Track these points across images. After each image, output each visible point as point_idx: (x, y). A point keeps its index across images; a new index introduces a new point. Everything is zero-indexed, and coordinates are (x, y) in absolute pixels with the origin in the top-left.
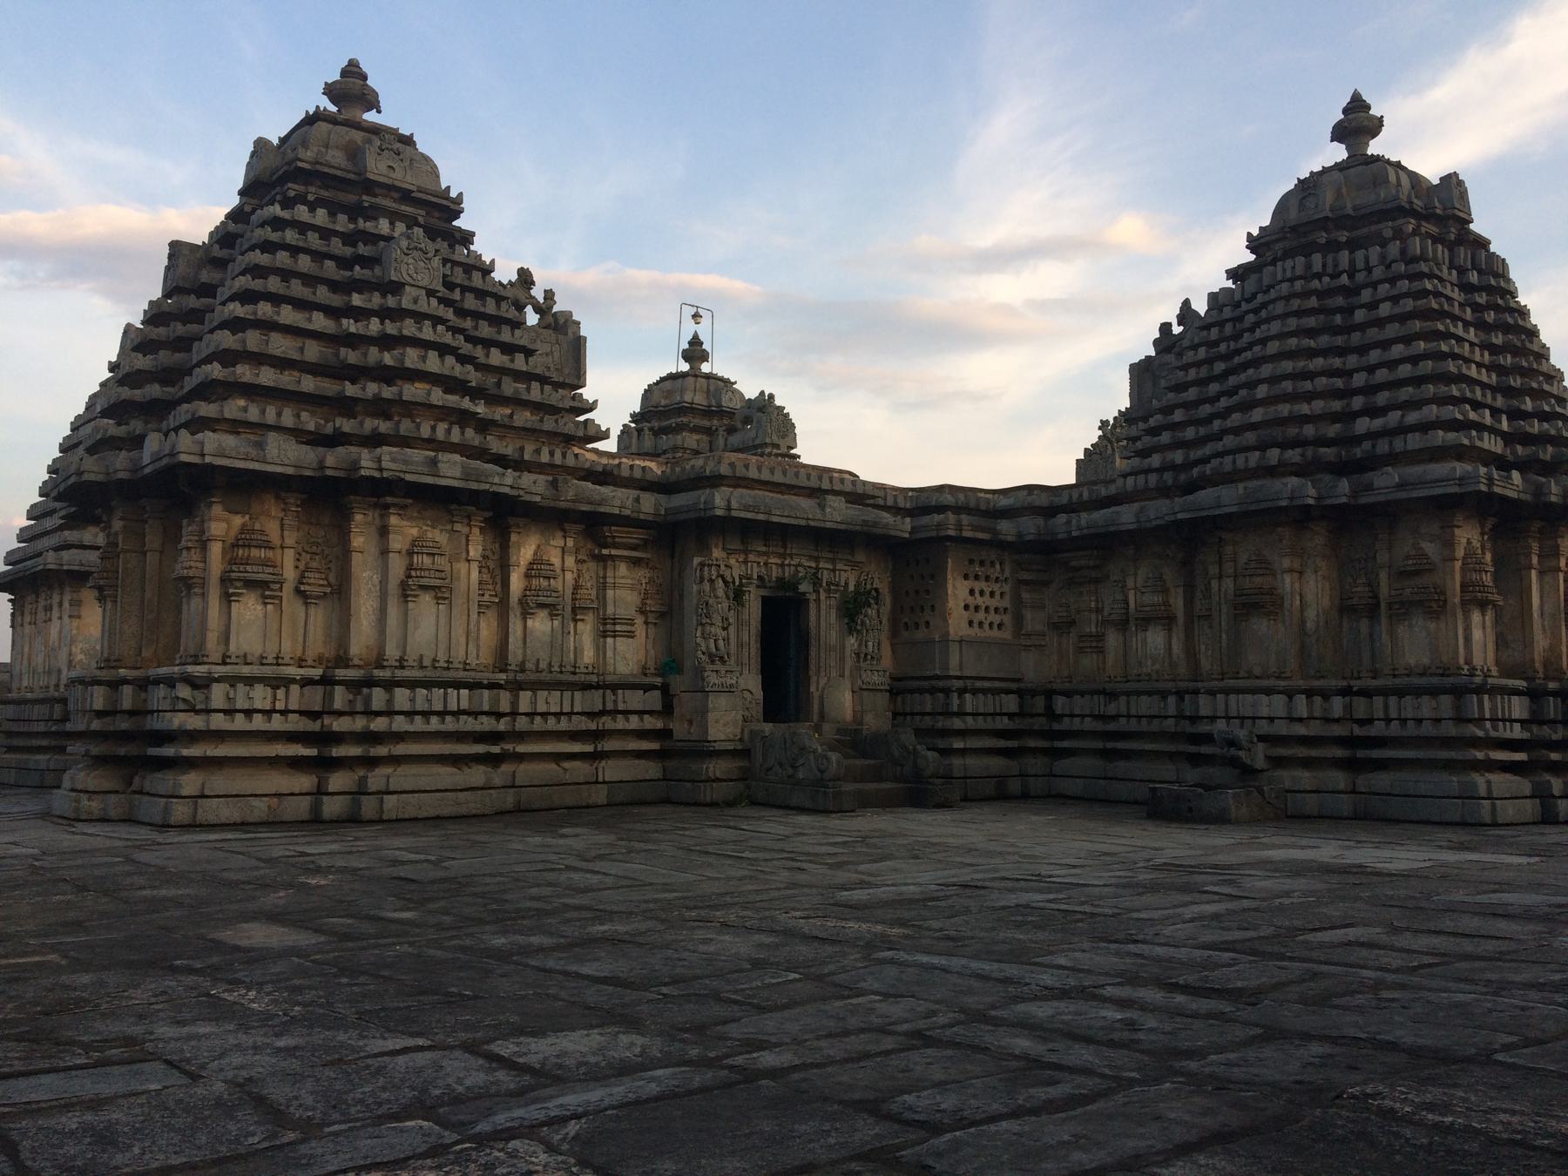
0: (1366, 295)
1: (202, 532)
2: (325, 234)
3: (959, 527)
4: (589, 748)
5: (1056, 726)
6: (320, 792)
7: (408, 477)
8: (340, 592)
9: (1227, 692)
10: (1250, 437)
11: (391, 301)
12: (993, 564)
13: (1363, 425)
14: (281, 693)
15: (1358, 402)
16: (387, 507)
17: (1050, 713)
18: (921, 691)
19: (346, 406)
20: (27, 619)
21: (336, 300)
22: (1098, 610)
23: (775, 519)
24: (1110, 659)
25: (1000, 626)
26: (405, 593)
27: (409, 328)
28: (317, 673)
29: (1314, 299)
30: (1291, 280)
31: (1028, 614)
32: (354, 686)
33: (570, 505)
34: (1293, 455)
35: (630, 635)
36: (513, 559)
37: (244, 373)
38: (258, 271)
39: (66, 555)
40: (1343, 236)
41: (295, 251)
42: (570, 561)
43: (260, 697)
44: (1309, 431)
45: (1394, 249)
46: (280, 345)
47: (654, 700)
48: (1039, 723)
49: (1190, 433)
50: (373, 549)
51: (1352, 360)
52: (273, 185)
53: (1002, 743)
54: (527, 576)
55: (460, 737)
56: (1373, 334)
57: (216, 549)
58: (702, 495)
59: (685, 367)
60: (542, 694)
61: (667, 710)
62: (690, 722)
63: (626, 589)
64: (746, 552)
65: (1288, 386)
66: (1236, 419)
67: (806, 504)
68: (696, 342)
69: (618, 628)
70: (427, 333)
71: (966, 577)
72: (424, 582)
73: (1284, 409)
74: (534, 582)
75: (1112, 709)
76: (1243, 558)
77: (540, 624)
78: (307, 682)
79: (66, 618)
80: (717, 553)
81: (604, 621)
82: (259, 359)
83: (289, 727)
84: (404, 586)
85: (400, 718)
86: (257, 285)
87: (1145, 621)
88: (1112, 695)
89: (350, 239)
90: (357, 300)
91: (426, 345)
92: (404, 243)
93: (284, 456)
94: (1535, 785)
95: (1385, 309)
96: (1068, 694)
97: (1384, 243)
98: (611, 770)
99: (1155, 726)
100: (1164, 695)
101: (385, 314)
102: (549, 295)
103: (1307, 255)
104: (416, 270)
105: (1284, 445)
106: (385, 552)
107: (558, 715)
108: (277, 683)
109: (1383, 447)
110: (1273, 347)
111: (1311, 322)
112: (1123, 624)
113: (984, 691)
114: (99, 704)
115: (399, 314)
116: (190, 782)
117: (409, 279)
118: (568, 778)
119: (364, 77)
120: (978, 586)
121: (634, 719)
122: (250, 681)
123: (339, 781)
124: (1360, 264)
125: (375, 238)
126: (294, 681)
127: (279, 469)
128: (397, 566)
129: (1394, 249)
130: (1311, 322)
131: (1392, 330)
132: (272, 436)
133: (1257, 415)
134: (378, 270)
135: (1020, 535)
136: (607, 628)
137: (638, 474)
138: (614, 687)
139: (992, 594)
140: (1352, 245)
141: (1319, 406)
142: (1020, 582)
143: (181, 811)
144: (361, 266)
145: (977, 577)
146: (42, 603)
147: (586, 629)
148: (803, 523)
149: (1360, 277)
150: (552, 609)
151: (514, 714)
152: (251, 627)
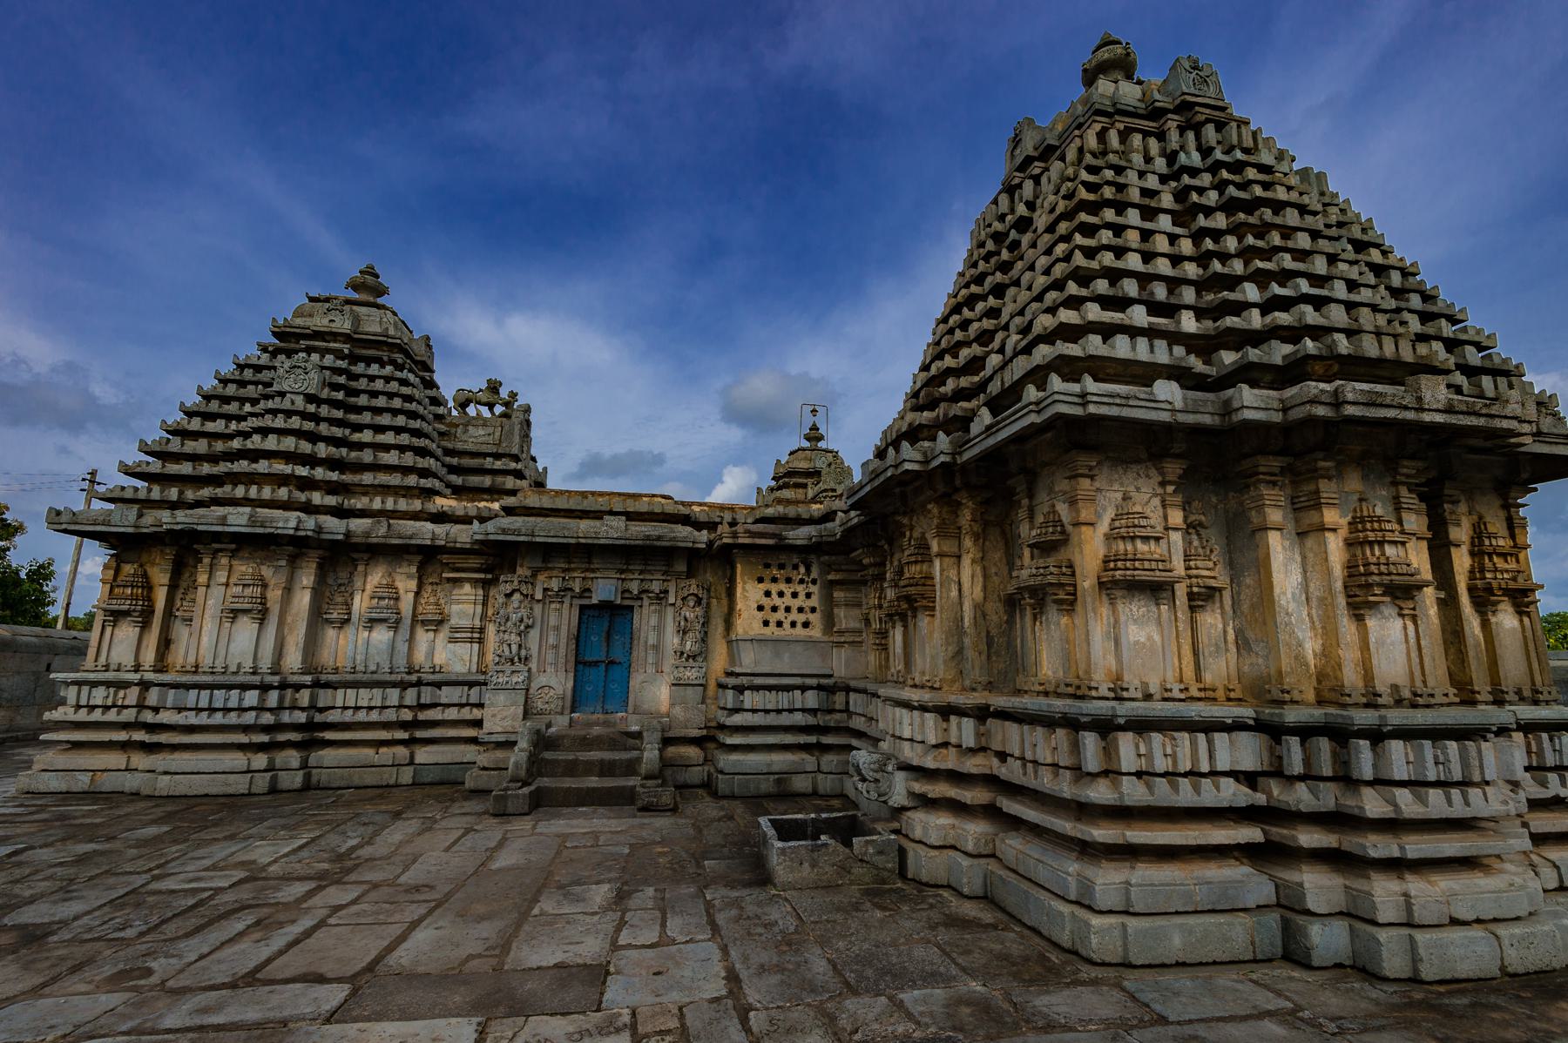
7: (200, 528)
12: (796, 567)
14: (121, 693)
23: (538, 539)
25: (806, 625)
31: (840, 612)
33: (382, 540)
53: (803, 739)
55: (246, 729)
59: (806, 444)
68: (814, 428)
78: (1237, 726)
102: (513, 395)
120: (774, 589)
122: (94, 684)
139: (795, 595)
142: (832, 582)
145: (774, 580)
148: (573, 541)
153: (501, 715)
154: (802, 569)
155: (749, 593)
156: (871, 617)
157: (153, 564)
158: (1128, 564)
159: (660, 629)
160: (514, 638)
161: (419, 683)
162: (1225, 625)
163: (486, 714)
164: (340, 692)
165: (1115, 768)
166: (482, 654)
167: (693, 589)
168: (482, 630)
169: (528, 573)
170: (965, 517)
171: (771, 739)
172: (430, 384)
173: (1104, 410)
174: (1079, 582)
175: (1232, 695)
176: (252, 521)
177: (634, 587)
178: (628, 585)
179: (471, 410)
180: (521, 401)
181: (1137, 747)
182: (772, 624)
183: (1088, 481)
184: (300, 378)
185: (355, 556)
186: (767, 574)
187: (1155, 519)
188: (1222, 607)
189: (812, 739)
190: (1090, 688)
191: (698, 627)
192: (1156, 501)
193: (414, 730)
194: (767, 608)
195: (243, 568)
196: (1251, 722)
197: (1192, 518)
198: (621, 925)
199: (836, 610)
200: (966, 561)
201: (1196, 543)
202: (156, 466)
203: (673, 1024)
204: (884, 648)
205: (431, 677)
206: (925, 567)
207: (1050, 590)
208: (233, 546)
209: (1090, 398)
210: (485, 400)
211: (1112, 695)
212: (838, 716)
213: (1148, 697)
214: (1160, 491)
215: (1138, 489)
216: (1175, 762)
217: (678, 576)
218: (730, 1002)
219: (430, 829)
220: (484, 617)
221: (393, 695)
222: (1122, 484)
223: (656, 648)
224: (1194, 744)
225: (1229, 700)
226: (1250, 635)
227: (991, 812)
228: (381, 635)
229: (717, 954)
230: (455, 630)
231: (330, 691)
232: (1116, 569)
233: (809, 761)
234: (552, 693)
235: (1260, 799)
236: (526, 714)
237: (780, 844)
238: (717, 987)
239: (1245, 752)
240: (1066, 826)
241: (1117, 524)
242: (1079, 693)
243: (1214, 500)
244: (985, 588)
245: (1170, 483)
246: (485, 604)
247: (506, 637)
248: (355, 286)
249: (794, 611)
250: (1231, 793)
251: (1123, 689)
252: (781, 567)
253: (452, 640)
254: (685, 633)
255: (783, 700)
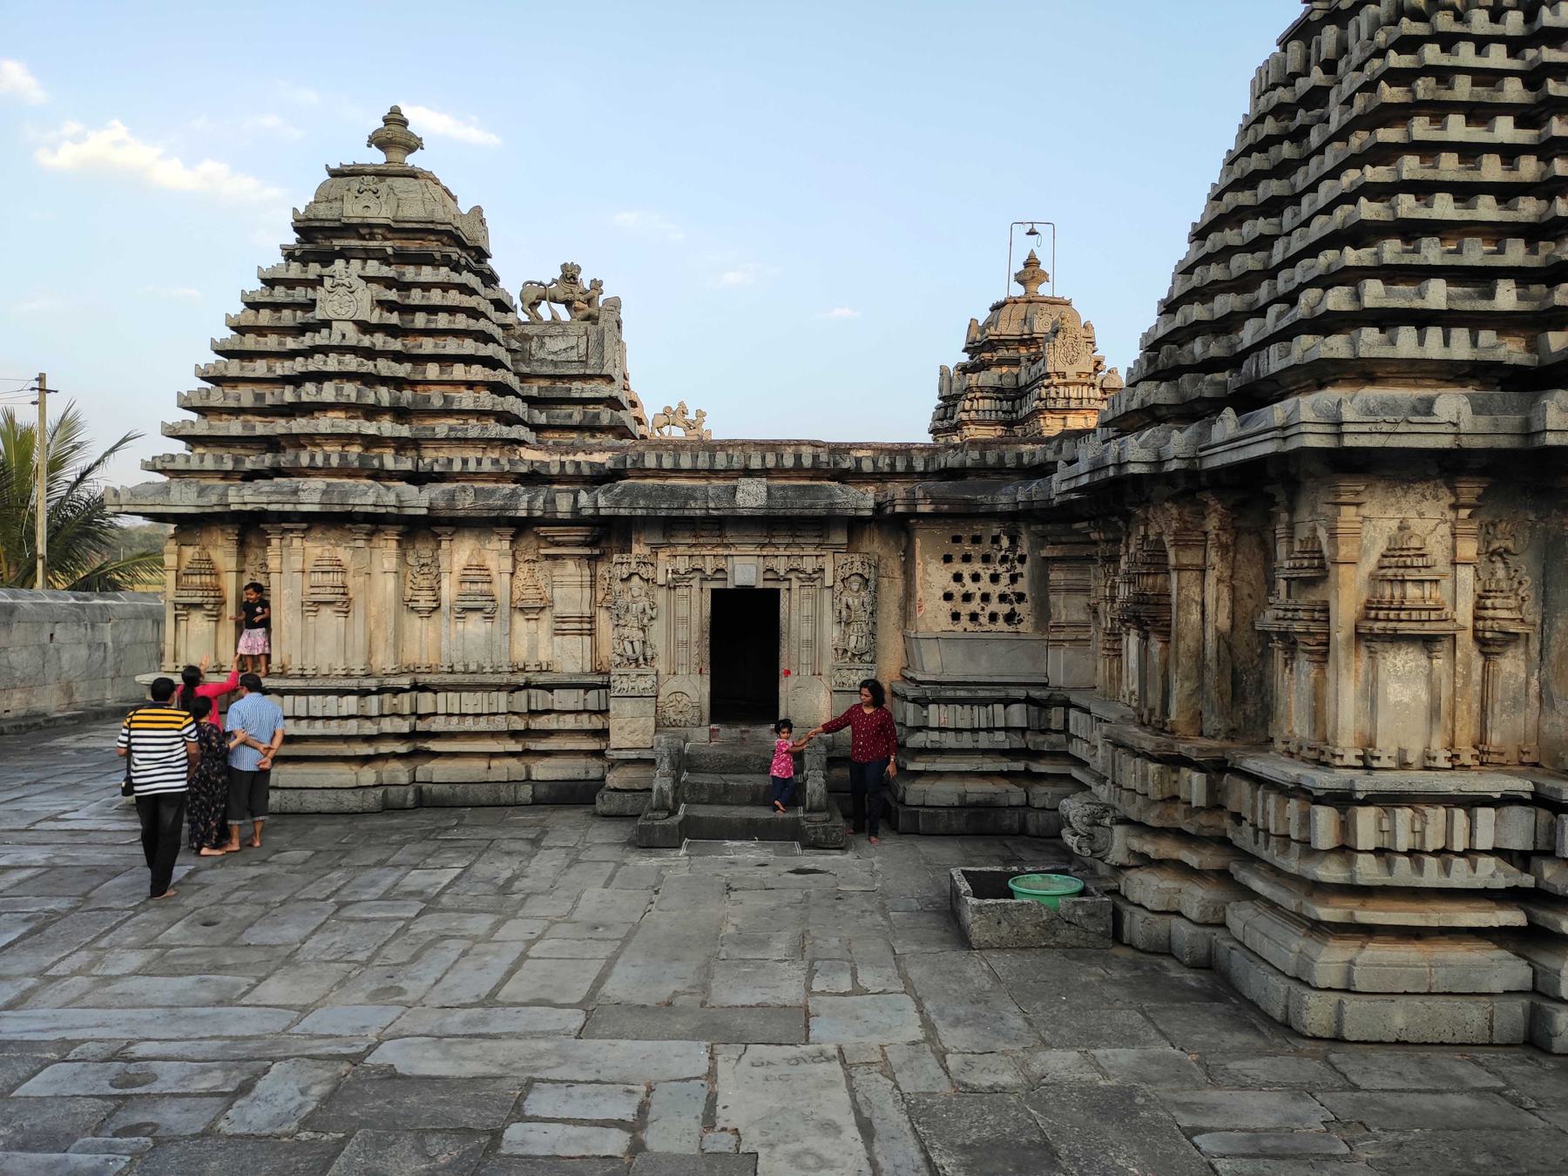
12: (996, 540)
25: (1010, 618)
29: (1270, 121)
36: (444, 565)
68: (1031, 262)
69: (578, 626)
71: (947, 559)
78: (1509, 800)
98: (543, 770)
117: (334, 316)
119: (405, 123)
120: (966, 570)
139: (995, 578)
142: (1046, 559)
145: (967, 559)
153: (630, 729)
154: (1005, 543)
155: (933, 576)
156: (1101, 609)
157: (216, 546)
158: (1392, 615)
159: (816, 619)
160: (637, 635)
161: (528, 685)
162: (1529, 674)
163: (613, 725)
164: (441, 696)
165: (1351, 844)
166: (595, 649)
167: (857, 568)
168: (592, 619)
169: (647, 551)
170: (1212, 524)
171: (964, 765)
172: (490, 279)
173: (1363, 442)
174: (1332, 632)
175: (1526, 759)
177: (781, 565)
178: (773, 563)
179: (544, 310)
180: (608, 292)
181: (1380, 823)
182: (965, 619)
183: (1353, 509)
184: (348, 297)
185: (438, 530)
186: (957, 551)
187: (1437, 549)
188: (1527, 653)
189: (1019, 766)
190: (1334, 756)
191: (865, 617)
192: (1445, 529)
193: (527, 739)
194: (958, 597)
195: (318, 551)
196: (1528, 796)
197: (1495, 545)
198: (811, 973)
199: (1052, 598)
200: (1211, 577)
201: (1501, 573)
202: (202, 427)
203: (877, 1058)
204: (1118, 654)
205: (542, 679)
206: (1160, 579)
207: (1299, 639)
208: (304, 525)
209: (1345, 428)
210: (561, 296)
211: (1360, 763)
212: (1054, 738)
213: (1404, 765)
214: (1450, 515)
215: (1421, 515)
216: (1423, 841)
217: (836, 549)
218: (927, 1047)
219: (577, 861)
220: (593, 602)
221: (501, 701)
222: (1400, 510)
223: (811, 644)
224: (1450, 820)
225: (1522, 764)
226: (1554, 689)
227: (1223, 876)
228: (475, 626)
229: (911, 1006)
230: (562, 619)
231: (429, 695)
232: (1377, 619)
233: (1015, 794)
234: (685, 700)
235: (1528, 881)
236: (659, 727)
237: (976, 901)
238: (916, 1033)
239: (1518, 830)
240: (1290, 901)
241: (1386, 562)
242: (1323, 759)
243: (1532, 517)
244: (1233, 615)
245: (1464, 506)
246: (593, 586)
247: (626, 631)
248: (378, 141)
249: (995, 599)
250: (1490, 873)
251: (1373, 758)
252: (976, 540)
253: (560, 632)
254: (848, 624)
255: (980, 716)
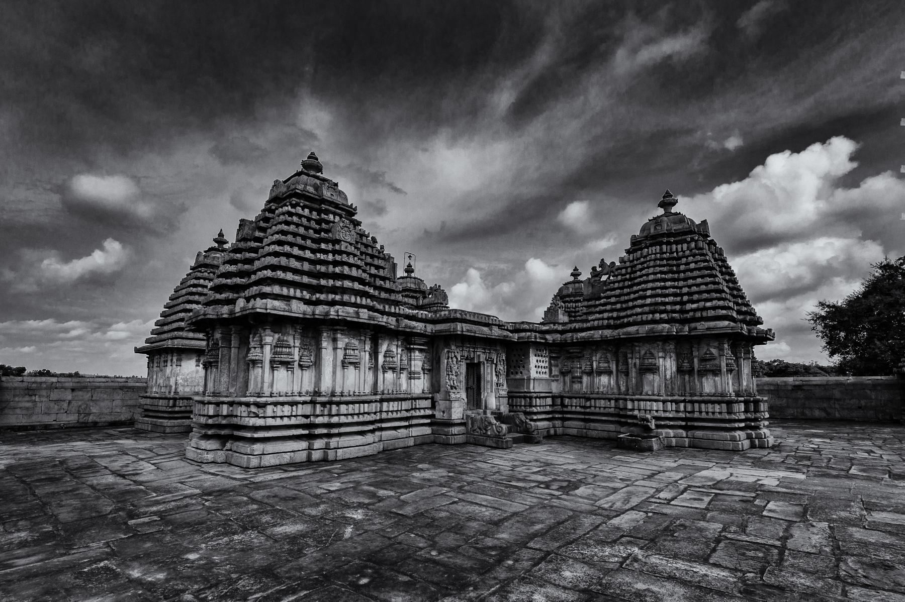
0: (684, 260)
1: (261, 341)
2: (309, 219)
3: (536, 338)
4: (406, 424)
5: (565, 409)
6: (310, 448)
8: (317, 364)
9: (639, 400)
10: (647, 309)
11: (337, 247)
13: (689, 306)
14: (294, 408)
15: (685, 298)
16: (337, 330)
17: (563, 405)
18: (520, 397)
19: (320, 289)
20: (155, 365)
21: (314, 246)
22: (580, 368)
24: (584, 385)
26: (344, 365)
27: (345, 258)
28: (308, 399)
30: (655, 254)
31: (553, 369)
32: (323, 404)
34: (664, 316)
35: (419, 378)
37: (280, 274)
38: (284, 233)
39: (176, 341)
40: (672, 240)
41: (297, 225)
42: (400, 350)
43: (287, 410)
44: (669, 307)
45: (693, 245)
46: (294, 264)
47: (427, 403)
48: (559, 408)
49: (618, 306)
50: (330, 348)
51: (681, 283)
52: (285, 199)
53: (548, 416)
54: (385, 357)
56: (689, 274)
57: (267, 348)
58: (452, 325)
59: (406, 275)
60: (391, 403)
61: (433, 407)
62: (444, 412)
63: (418, 362)
64: (463, 347)
65: (659, 291)
66: (640, 302)
67: (485, 329)
68: (409, 266)
70: (351, 260)
72: (351, 360)
73: (659, 300)
74: (388, 359)
75: (588, 404)
76: (643, 352)
77: (390, 375)
78: (304, 403)
79: (174, 366)
80: (453, 347)
81: (410, 373)
82: (285, 269)
83: (298, 422)
84: (343, 362)
85: (342, 417)
86: (283, 238)
87: (600, 373)
88: (589, 399)
89: (318, 222)
90: (323, 246)
91: (350, 265)
92: (341, 224)
93: (298, 309)
94: (747, 434)
95: (692, 266)
96: (570, 398)
97: (688, 243)
99: (607, 411)
100: (610, 400)
101: (334, 252)
102: (382, 247)
103: (661, 245)
104: (347, 236)
105: (661, 312)
106: (335, 349)
107: (397, 411)
108: (292, 404)
109: (698, 315)
110: (651, 277)
111: (665, 269)
112: (590, 373)
113: (543, 397)
114: (211, 413)
115: (340, 252)
116: (258, 448)
118: (400, 435)
121: (422, 411)
123: (319, 444)
124: (680, 250)
125: (328, 222)
126: (299, 403)
127: (297, 315)
128: (340, 354)
129: (693, 245)
130: (665, 269)
131: (696, 273)
132: (294, 302)
133: (648, 301)
134: (330, 235)
135: (554, 340)
136: (412, 376)
137: (424, 317)
138: (415, 399)
140: (676, 243)
141: (671, 299)
143: (254, 462)
144: (322, 235)
146: (162, 359)
147: (404, 376)
149: (681, 254)
150: (393, 369)
151: (381, 411)
152: (283, 382)
176: (370, 318)
